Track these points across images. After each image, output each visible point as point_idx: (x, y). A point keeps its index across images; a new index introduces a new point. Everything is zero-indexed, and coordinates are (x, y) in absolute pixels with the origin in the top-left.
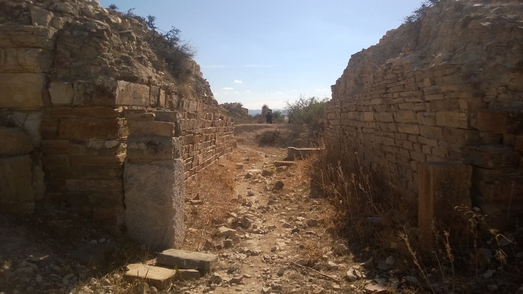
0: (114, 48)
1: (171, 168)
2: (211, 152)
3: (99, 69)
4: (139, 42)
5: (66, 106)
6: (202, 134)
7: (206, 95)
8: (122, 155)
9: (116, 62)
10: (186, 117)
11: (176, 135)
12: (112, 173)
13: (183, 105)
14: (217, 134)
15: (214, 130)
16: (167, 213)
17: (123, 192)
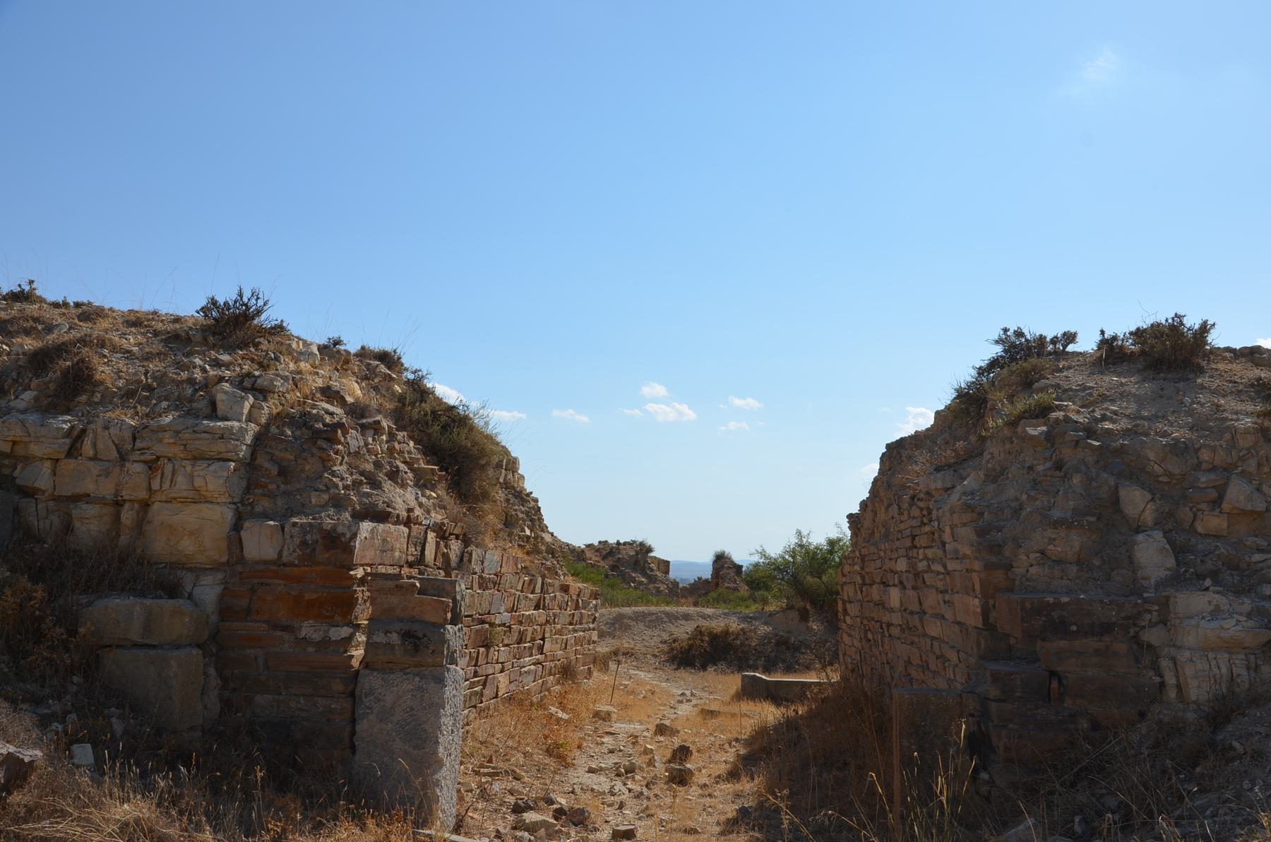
0: (349, 454)
1: (441, 681)
2: (528, 672)
3: (326, 497)
4: (392, 436)
5: (265, 562)
6: (509, 627)
7: (528, 532)
8: (358, 653)
9: (354, 482)
11: (454, 622)
12: (338, 686)
13: (470, 561)
15: (542, 619)
16: (427, 762)
17: (353, 721)
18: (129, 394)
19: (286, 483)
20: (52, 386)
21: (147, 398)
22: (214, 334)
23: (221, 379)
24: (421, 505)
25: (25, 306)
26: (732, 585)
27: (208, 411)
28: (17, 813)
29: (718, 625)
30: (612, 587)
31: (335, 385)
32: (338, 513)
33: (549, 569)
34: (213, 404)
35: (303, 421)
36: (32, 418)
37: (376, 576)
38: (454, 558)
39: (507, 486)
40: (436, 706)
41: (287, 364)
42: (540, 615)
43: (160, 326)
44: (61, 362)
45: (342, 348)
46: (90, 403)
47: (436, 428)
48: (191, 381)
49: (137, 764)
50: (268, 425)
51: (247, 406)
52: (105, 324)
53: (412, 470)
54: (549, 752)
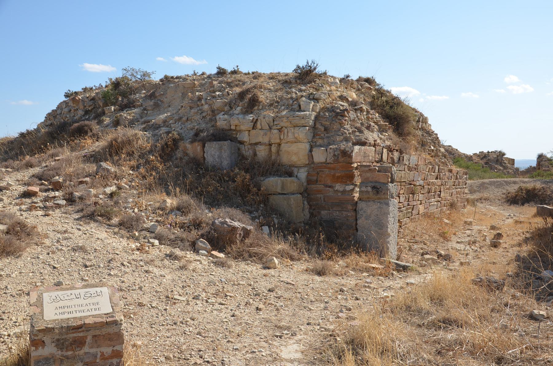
0: (351, 121)
1: (388, 204)
2: (434, 205)
3: (342, 137)
4: (368, 112)
5: (321, 163)
7: (432, 148)
8: (356, 195)
9: (353, 131)
10: (406, 170)
11: (392, 182)
12: (350, 207)
13: (403, 160)
14: (442, 187)
15: (440, 183)
17: (356, 220)
18: (271, 105)
19: (327, 133)
20: (246, 104)
21: (277, 106)
22: (299, 79)
23: (302, 96)
24: (381, 139)
25: (236, 75)
26: (547, 169)
27: (298, 109)
28: (247, 245)
29: (530, 186)
30: (485, 172)
31: (345, 94)
32: (347, 143)
33: (442, 163)
34: (300, 106)
35: (332, 109)
36: (241, 116)
37: (361, 166)
38: (396, 159)
39: (422, 129)
40: (387, 214)
41: (326, 88)
42: (439, 182)
43: (280, 78)
44: (248, 96)
45: (350, 78)
46: (258, 109)
47: (388, 107)
48: (292, 98)
49: (282, 232)
50: (319, 112)
51: (311, 105)
52: (262, 79)
53: (378, 125)
54: (440, 235)
